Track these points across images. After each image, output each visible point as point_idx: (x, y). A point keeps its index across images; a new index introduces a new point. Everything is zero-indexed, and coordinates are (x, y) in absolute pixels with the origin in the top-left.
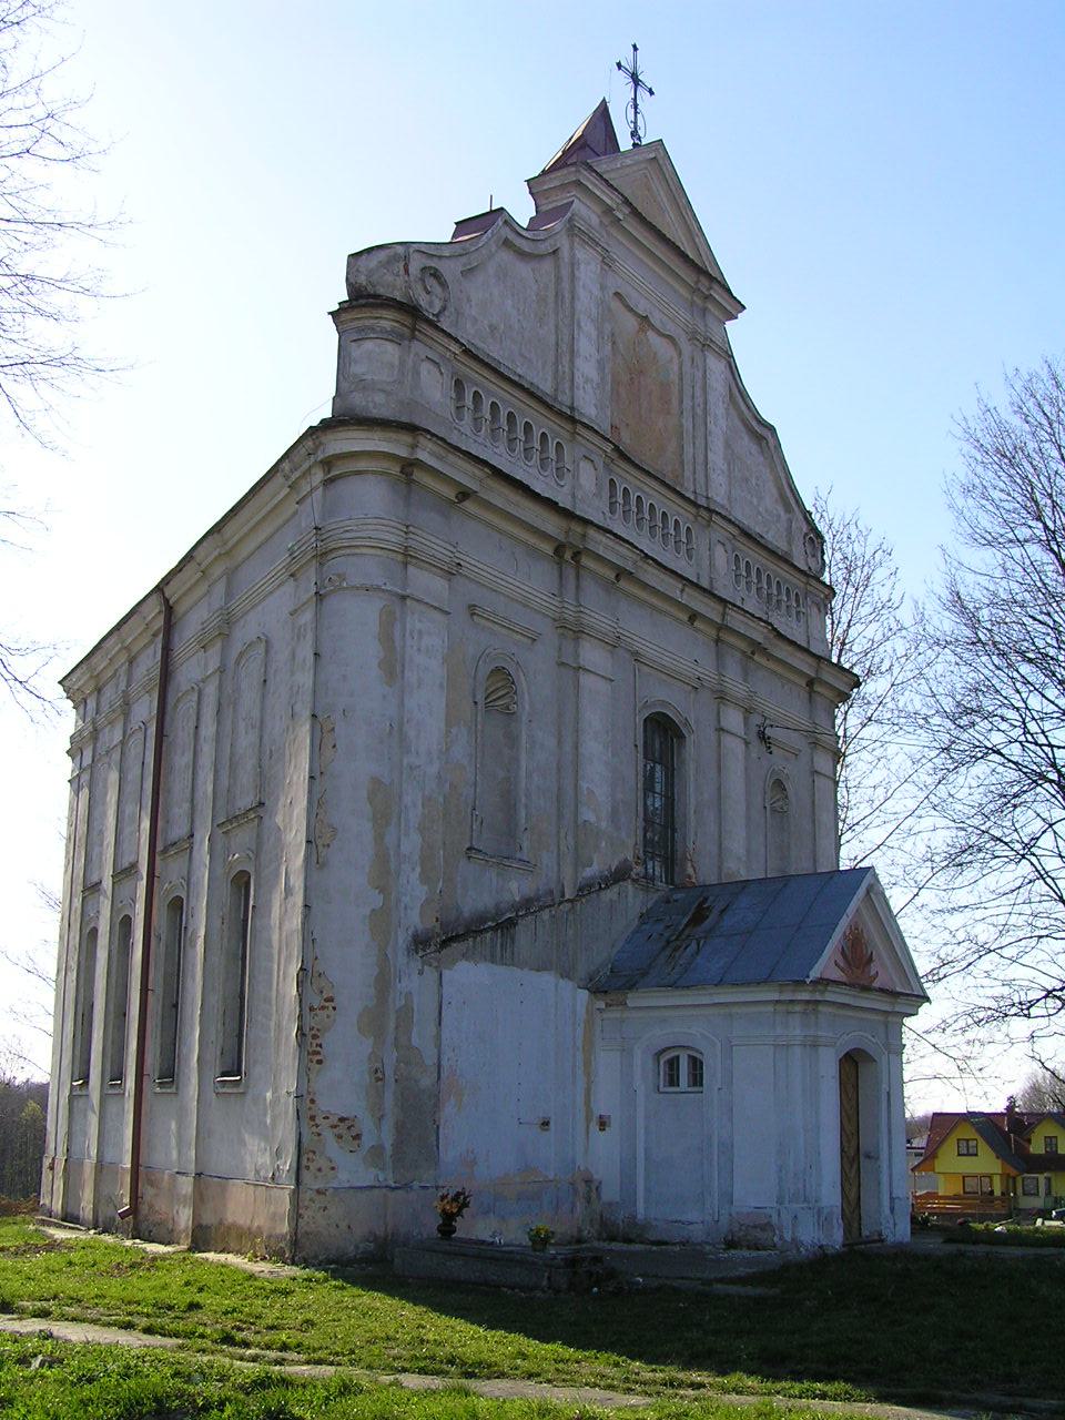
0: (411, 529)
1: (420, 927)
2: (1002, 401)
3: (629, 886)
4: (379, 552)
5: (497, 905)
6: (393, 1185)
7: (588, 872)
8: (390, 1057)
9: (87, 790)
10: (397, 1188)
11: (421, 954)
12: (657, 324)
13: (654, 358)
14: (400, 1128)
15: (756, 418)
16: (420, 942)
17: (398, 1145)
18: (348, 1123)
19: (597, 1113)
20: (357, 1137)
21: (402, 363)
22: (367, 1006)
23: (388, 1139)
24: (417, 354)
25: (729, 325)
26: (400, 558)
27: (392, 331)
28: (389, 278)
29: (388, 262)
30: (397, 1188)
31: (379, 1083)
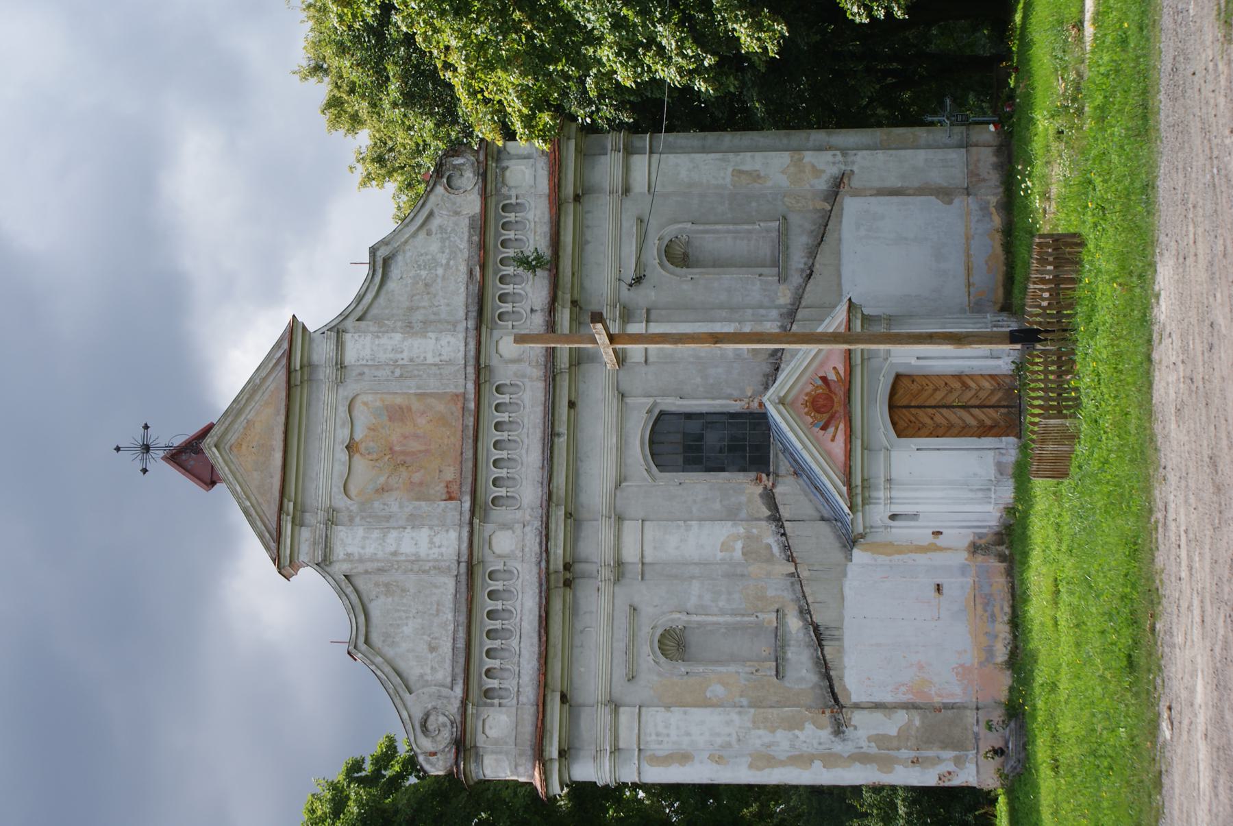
0: (598, 749)
1: (829, 730)
2: (342, 132)
3: (778, 490)
4: (617, 768)
5: (808, 646)
6: (975, 751)
7: (776, 550)
8: (905, 754)
9: (574, 140)
10: (978, 748)
11: (844, 728)
12: (347, 432)
13: (373, 430)
14: (945, 746)
15: (373, 275)
16: (839, 729)
17: (955, 748)
18: (942, 777)
19: (930, 539)
20: (949, 773)
21: (493, 752)
22: (878, 770)
23: (949, 754)
24: (485, 743)
25: (311, 328)
26: (617, 754)
27: (476, 762)
28: (441, 763)
29: (431, 764)
30: (978, 748)
31: (920, 760)
